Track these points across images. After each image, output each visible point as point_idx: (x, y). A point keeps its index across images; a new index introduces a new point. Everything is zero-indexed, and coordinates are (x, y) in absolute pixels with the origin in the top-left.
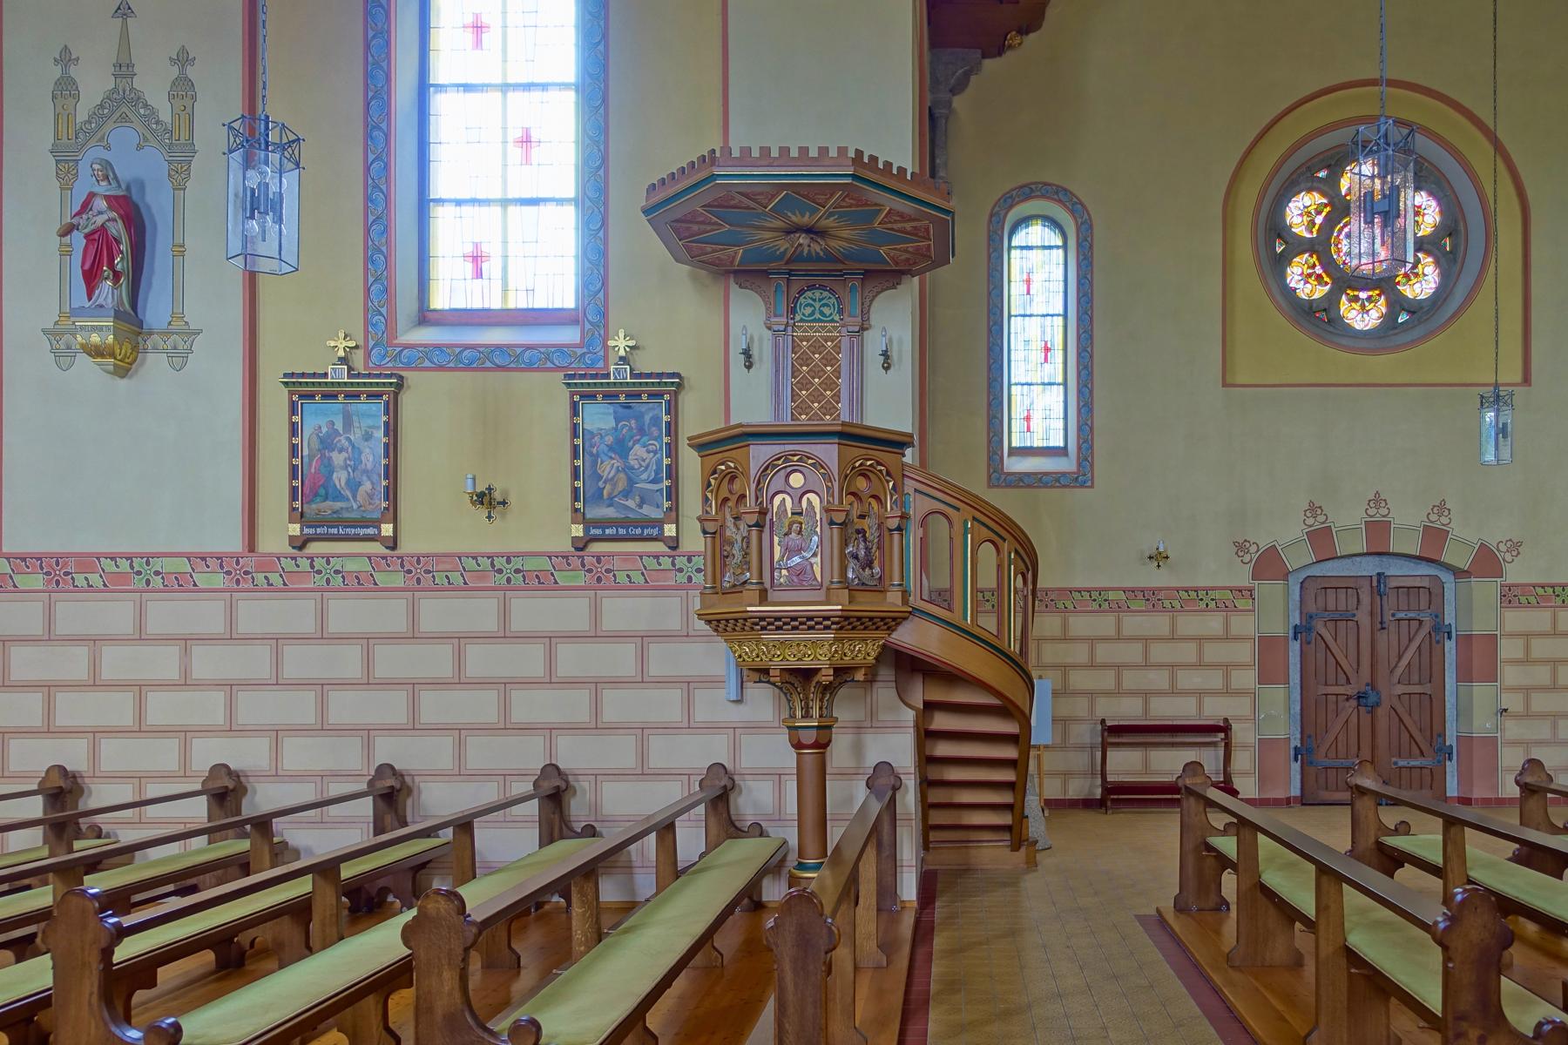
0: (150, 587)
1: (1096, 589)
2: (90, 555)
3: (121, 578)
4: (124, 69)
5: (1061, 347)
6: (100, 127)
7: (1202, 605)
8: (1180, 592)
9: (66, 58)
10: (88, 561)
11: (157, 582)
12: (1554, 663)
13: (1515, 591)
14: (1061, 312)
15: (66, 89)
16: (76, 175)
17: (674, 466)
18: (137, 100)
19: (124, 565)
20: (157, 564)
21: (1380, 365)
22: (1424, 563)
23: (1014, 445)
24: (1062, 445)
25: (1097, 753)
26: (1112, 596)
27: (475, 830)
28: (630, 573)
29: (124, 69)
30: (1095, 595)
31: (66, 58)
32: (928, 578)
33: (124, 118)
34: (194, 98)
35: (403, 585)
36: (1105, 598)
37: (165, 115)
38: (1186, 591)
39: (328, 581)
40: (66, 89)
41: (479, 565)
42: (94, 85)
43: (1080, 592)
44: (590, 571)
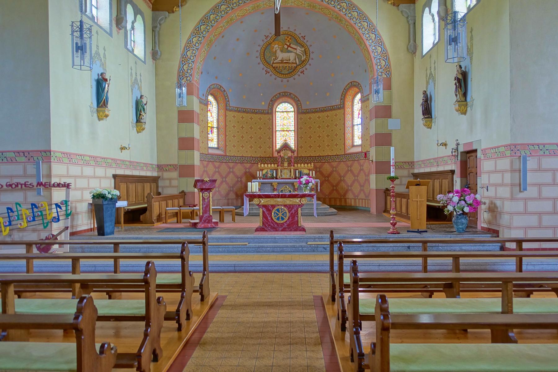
0: (3, 161)
1: (542, 144)
8: (20, 153)
11: (547, 153)
12: (554, 171)
13: (519, 147)
21: (15, 189)
22: (167, 271)
23: (81, 260)
25: (123, 171)
26: (8, 155)
27: (445, 170)
28: (534, 149)
30: (541, 147)
35: (24, 161)
36: (5, 156)
38: (45, 152)
39: (544, 153)
41: (534, 148)
43: (533, 145)
44: (26, 157)
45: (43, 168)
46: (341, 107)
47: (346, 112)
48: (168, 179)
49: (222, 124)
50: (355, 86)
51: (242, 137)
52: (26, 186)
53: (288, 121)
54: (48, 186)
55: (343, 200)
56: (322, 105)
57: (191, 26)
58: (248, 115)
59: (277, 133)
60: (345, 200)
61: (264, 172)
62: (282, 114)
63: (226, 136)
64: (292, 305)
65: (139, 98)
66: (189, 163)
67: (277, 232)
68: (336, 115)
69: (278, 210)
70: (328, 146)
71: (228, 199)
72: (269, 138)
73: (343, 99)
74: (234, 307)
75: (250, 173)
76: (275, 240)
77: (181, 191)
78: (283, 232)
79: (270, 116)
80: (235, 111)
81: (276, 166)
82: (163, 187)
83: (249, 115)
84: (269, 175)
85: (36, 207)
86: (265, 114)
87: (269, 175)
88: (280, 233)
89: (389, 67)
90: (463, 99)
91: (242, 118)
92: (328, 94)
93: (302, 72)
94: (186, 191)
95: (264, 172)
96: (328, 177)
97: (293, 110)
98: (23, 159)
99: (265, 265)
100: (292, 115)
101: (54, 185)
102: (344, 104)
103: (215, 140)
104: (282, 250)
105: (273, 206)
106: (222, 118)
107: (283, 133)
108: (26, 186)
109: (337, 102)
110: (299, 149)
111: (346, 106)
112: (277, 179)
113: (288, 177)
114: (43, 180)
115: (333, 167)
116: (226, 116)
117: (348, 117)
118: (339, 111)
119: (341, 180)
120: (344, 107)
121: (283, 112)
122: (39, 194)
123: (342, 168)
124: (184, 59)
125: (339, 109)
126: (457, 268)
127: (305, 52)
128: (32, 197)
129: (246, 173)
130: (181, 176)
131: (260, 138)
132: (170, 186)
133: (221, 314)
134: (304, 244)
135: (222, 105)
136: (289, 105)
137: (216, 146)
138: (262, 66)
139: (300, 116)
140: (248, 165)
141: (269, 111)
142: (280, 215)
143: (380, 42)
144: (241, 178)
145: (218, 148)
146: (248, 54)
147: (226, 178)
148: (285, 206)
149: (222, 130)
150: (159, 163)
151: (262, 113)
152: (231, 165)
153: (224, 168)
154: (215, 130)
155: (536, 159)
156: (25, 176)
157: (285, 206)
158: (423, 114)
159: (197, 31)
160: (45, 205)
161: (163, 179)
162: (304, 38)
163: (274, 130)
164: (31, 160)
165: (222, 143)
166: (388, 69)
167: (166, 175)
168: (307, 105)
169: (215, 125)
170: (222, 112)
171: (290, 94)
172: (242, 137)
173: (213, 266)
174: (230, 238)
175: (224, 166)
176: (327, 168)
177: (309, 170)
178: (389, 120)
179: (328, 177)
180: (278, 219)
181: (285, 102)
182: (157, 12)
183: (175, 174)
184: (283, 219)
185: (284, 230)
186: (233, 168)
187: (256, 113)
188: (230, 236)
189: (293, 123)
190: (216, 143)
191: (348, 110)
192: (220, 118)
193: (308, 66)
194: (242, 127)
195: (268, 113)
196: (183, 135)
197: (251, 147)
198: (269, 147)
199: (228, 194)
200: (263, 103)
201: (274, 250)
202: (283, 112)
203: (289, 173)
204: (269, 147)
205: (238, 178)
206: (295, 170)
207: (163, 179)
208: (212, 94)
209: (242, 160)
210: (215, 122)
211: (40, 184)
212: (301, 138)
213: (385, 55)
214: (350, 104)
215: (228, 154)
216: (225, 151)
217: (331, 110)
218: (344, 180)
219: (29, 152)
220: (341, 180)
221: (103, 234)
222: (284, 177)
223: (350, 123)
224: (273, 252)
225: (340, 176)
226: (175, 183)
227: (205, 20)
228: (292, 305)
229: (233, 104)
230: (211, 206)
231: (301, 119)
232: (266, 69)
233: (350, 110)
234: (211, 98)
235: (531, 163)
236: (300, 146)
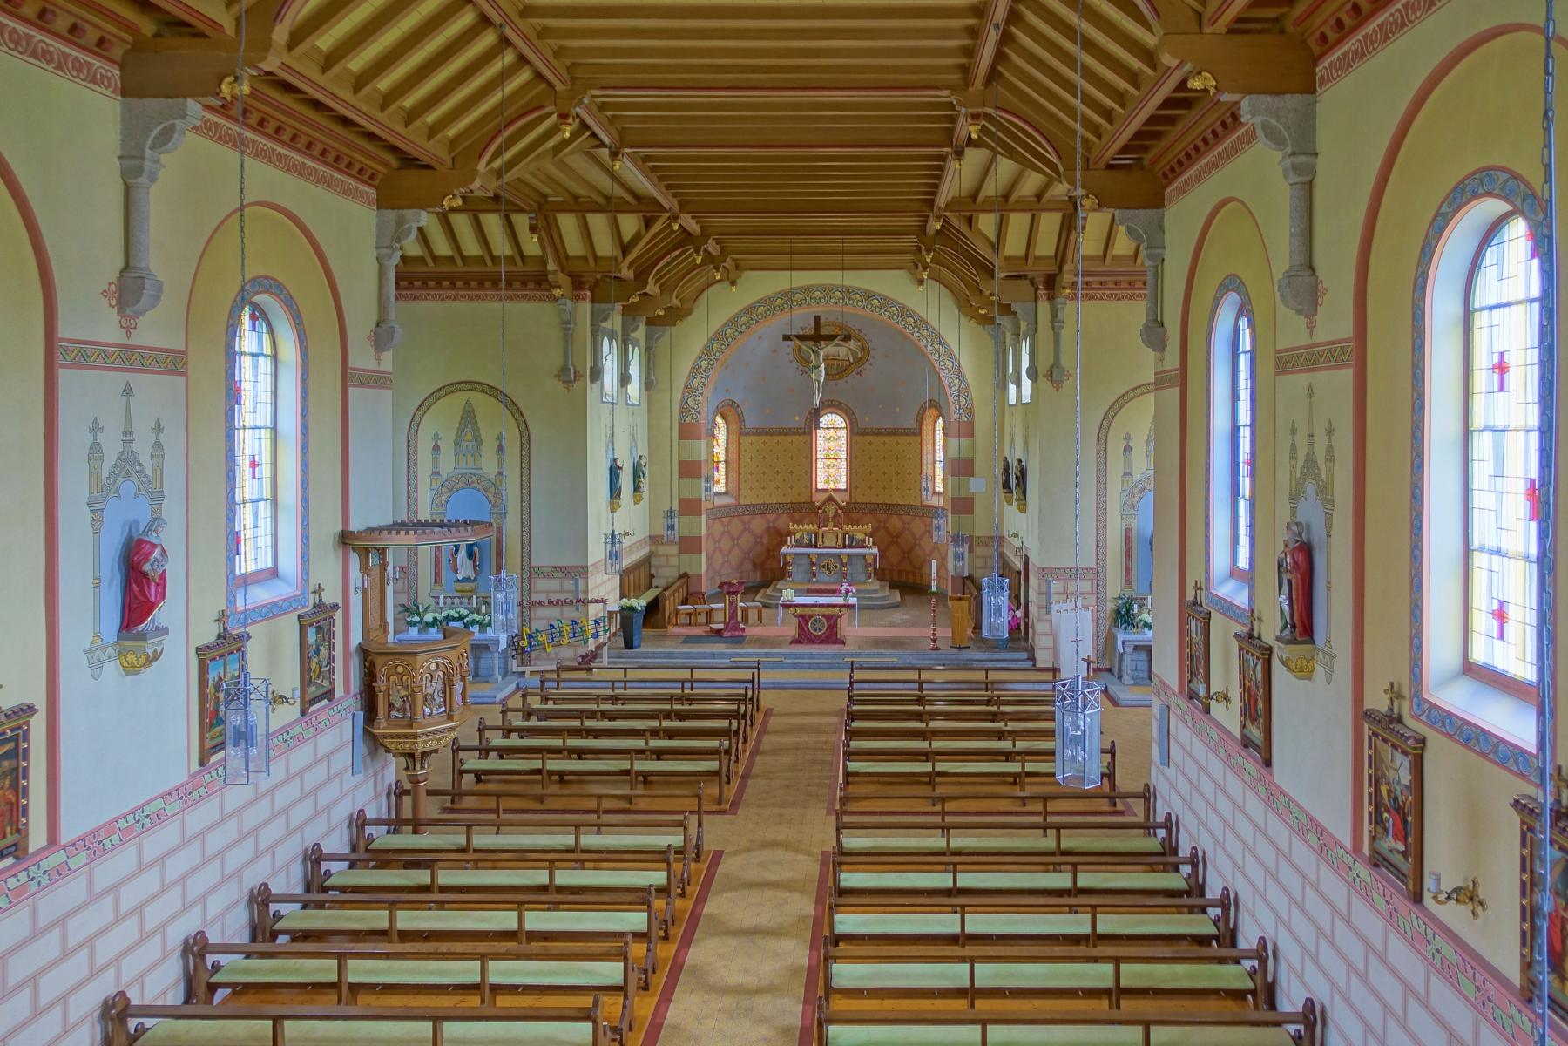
2: (110, 823)
3: (130, 829)
4: (128, 438)
5: (269, 461)
6: (115, 482)
7: (138, 829)
9: (96, 428)
10: (109, 827)
13: (1046, 571)
14: (269, 424)
15: (96, 451)
16: (102, 521)
17: (1101, 570)
18: (135, 460)
19: (130, 818)
20: (148, 810)
24: (270, 565)
26: (544, 570)
29: (128, 438)
31: (96, 428)
32: (1251, 324)
33: (128, 474)
34: (163, 457)
37: (149, 472)
40: (96, 451)
42: (112, 449)
45: (581, 583)
46: (918, 432)
47: (924, 442)
48: (663, 556)
49: (733, 456)
50: (935, 407)
51: (764, 473)
52: (565, 602)
53: (836, 443)
54: (586, 602)
55: (918, 576)
56: (887, 424)
57: (698, 344)
58: (774, 437)
59: (819, 462)
60: (921, 574)
61: (798, 536)
62: (827, 431)
63: (739, 474)
64: (822, 714)
65: (637, 459)
66: (694, 534)
67: (813, 646)
68: (910, 443)
69: (816, 620)
70: (897, 489)
71: (741, 572)
72: (806, 473)
73: (920, 421)
74: (781, 715)
75: (774, 528)
76: (811, 656)
77: (682, 572)
78: (820, 646)
79: (808, 437)
80: (754, 434)
81: (816, 527)
82: (657, 567)
83: (776, 438)
84: (805, 541)
85: (576, 623)
86: (800, 434)
87: (805, 541)
88: (817, 646)
89: (972, 407)
90: (1022, 497)
91: (764, 443)
92: (898, 410)
93: (858, 373)
94: (689, 572)
95: (798, 536)
96: (897, 537)
97: (843, 425)
98: (560, 574)
99: (802, 683)
100: (843, 432)
101: (592, 602)
102: (921, 429)
103: (723, 481)
104: (818, 667)
105: (810, 616)
106: (733, 447)
107: (828, 462)
108: (565, 602)
109: (910, 423)
110: (854, 490)
111: (924, 432)
112: (816, 547)
113: (834, 545)
114: (581, 596)
115: (904, 523)
116: (739, 443)
117: (927, 449)
118: (914, 438)
119: (915, 544)
120: (920, 434)
121: (828, 428)
122: (577, 610)
123: (917, 526)
124: (689, 390)
125: (914, 434)
126: (921, 689)
127: (863, 347)
128: (569, 612)
129: (768, 530)
130: (682, 551)
131: (792, 473)
132: (668, 566)
133: (773, 720)
134: (841, 660)
135: (734, 427)
136: (838, 417)
137: (723, 490)
138: (795, 364)
139: (859, 438)
140: (771, 517)
141: (807, 430)
142: (818, 625)
143: (959, 373)
144: (761, 538)
145: (726, 493)
146: (775, 351)
147: (738, 539)
148: (823, 616)
149: (734, 466)
150: (653, 534)
151: (794, 434)
152: (746, 518)
153: (736, 526)
154: (722, 466)
155: (1062, 583)
156: (561, 591)
157: (823, 616)
158: (1003, 487)
159: (707, 352)
160: (584, 620)
161: (658, 556)
162: (860, 331)
163: (814, 459)
164: (568, 575)
165: (733, 486)
166: (970, 410)
167: (662, 550)
168: (866, 421)
169: (722, 458)
170: (733, 437)
171: (840, 403)
172: (764, 473)
173: (765, 683)
174: (766, 653)
175: (736, 521)
176: (895, 523)
177: (866, 534)
178: (971, 479)
179: (897, 537)
180: (815, 630)
181: (832, 413)
182: (653, 328)
183: (674, 550)
184: (820, 630)
185: (822, 642)
186: (749, 523)
187: (786, 434)
188: (766, 651)
189: (845, 446)
190: (723, 485)
191: (927, 438)
192: (730, 446)
193: (866, 366)
194: (764, 458)
195: (804, 433)
196: (687, 495)
197: (777, 488)
198: (806, 487)
199: (741, 564)
200: (797, 418)
201: (810, 667)
202: (828, 428)
203: (835, 539)
204: (806, 487)
205: (756, 537)
206: (844, 535)
207: (658, 556)
208: (723, 417)
209: (764, 509)
210: (723, 452)
211: (578, 601)
212: (856, 472)
213: (964, 390)
214: (930, 428)
215: (741, 503)
216: (738, 499)
217: (902, 434)
218: (919, 544)
219: (566, 568)
220: (915, 544)
221: (632, 648)
222: (827, 544)
223: (930, 458)
224: (810, 668)
225: (915, 539)
226: (674, 561)
227: (719, 336)
228: (822, 714)
229: (750, 423)
230: (483, 269)
231: (857, 443)
232: (801, 367)
233: (930, 438)
234: (719, 419)
235: (1056, 586)
236: (854, 485)
